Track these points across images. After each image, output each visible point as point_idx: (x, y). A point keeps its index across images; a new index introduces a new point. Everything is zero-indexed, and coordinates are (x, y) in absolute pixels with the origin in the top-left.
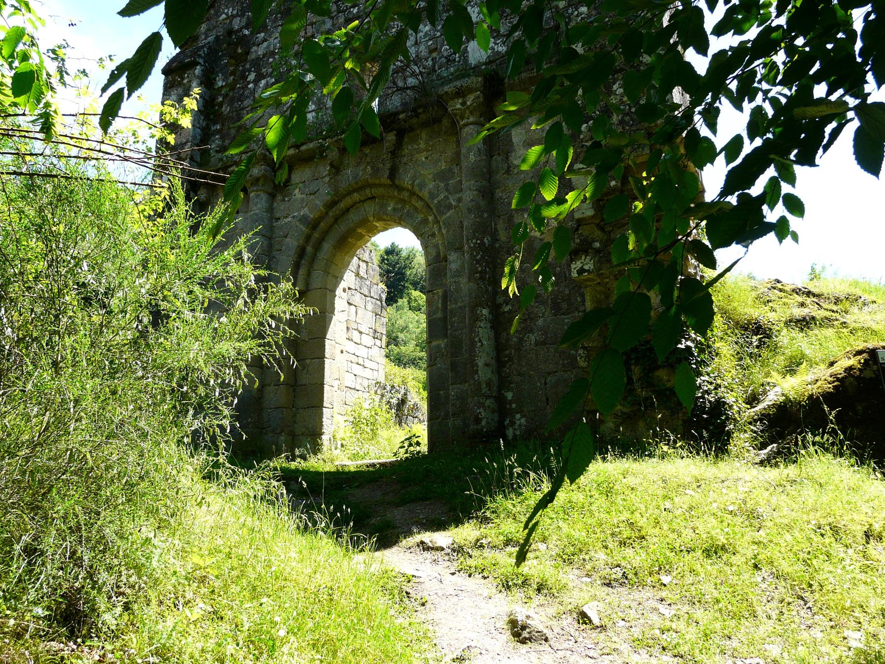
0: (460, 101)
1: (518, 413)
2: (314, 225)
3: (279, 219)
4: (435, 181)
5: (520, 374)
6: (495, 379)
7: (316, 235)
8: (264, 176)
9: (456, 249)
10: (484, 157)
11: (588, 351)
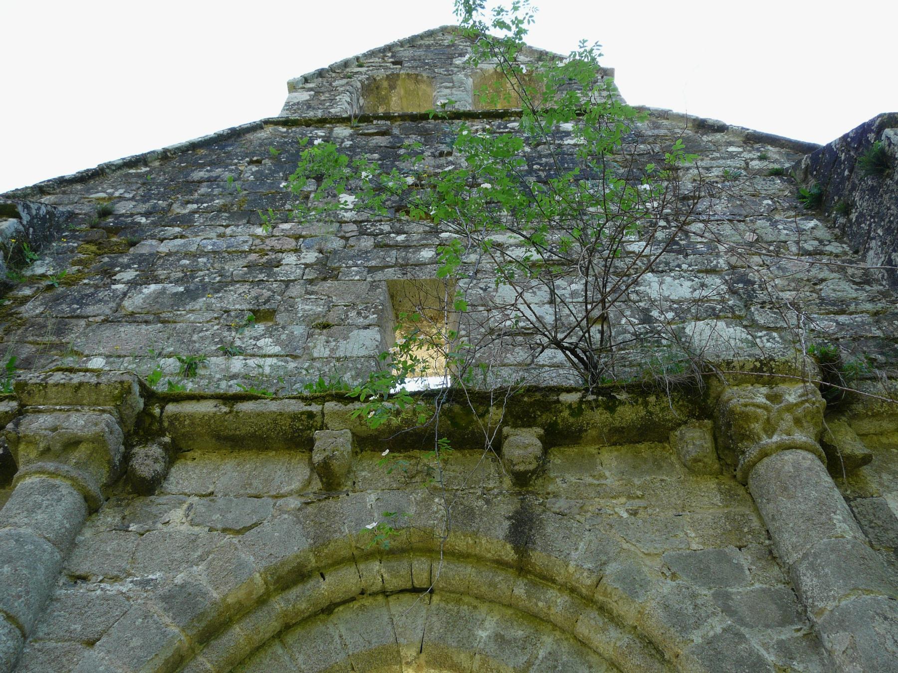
3: (84, 579)
4: (674, 576)
8: (98, 440)
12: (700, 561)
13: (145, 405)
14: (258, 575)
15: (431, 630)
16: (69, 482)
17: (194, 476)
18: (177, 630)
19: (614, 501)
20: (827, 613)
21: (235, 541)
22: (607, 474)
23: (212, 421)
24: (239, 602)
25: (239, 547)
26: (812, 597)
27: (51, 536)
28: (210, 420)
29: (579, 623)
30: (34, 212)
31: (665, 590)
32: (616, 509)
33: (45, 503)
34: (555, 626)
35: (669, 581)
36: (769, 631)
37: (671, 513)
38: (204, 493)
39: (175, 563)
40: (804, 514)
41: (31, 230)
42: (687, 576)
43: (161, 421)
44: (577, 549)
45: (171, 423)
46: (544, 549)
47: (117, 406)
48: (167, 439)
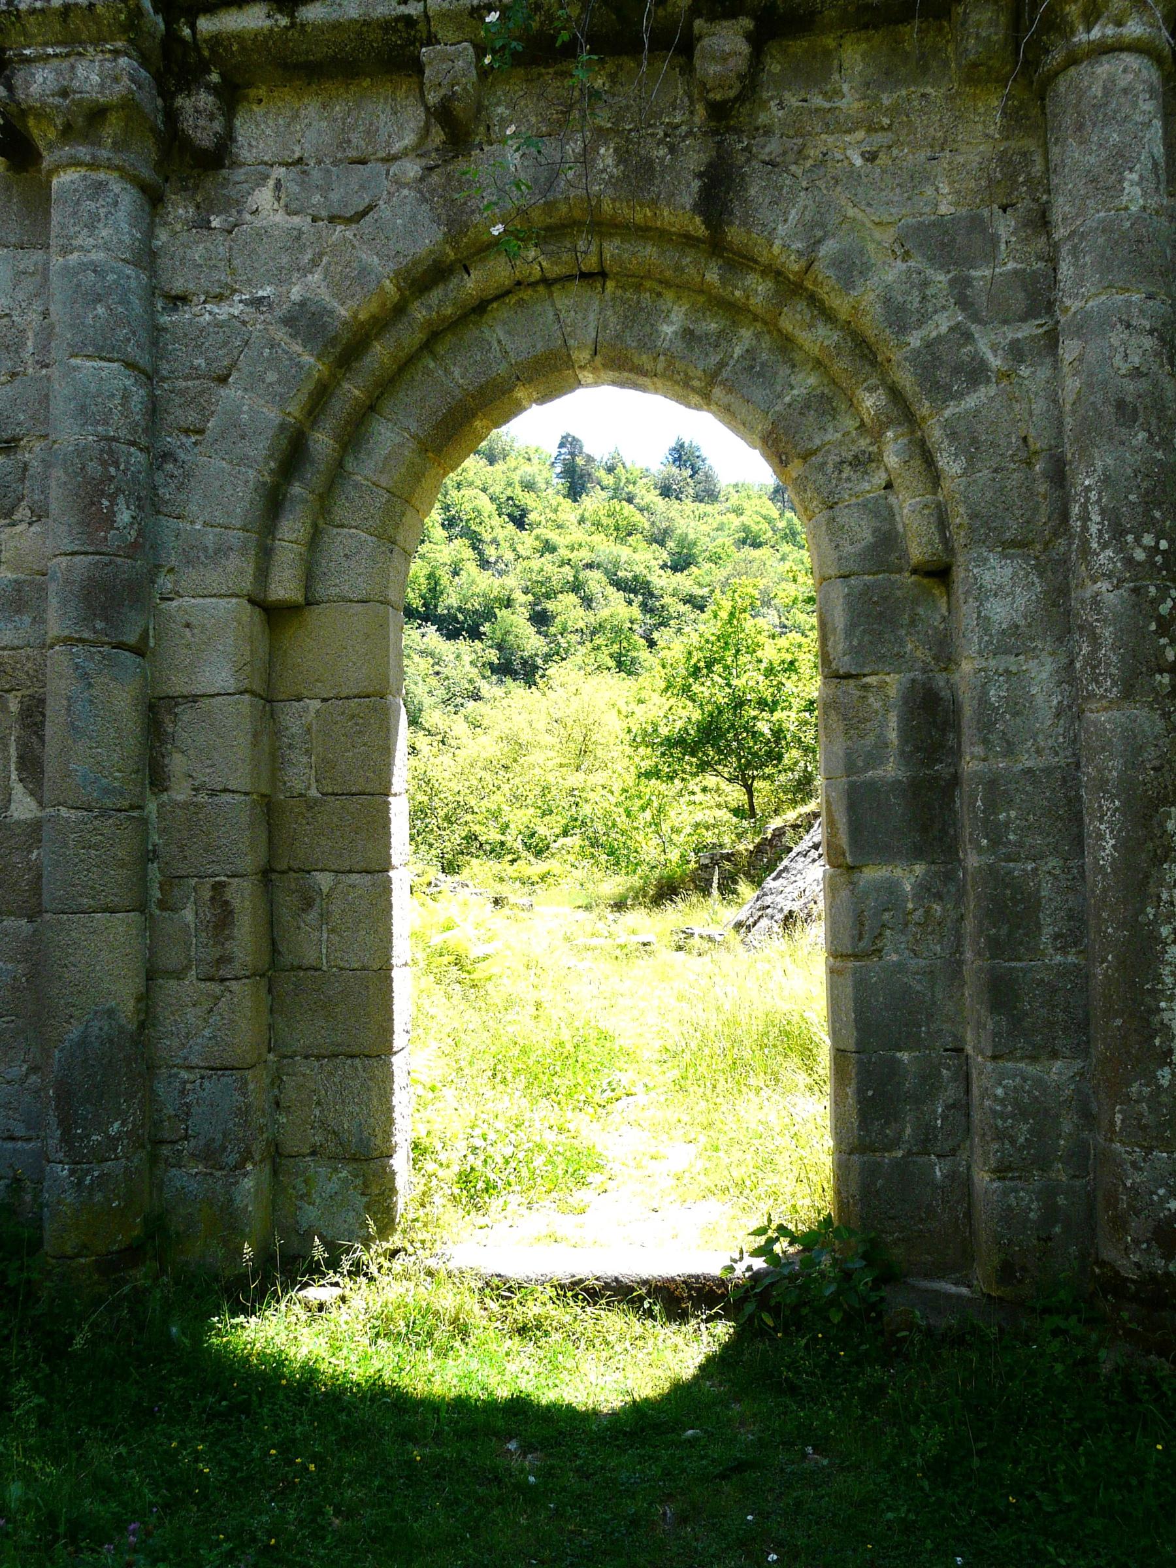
4: (907, 256)
7: (353, 390)
8: (128, 105)
9: (1006, 545)
12: (946, 233)
13: (168, 23)
14: (388, 282)
15: (605, 327)
16: (116, 174)
17: (269, 131)
18: (312, 360)
19: (847, 138)
20: (1070, 314)
21: (349, 235)
22: (845, 87)
23: (271, 42)
24: (373, 317)
25: (356, 243)
26: (1063, 291)
27: (127, 256)
28: (267, 42)
29: (783, 317)
31: (890, 278)
32: (849, 152)
33: (102, 211)
34: (756, 318)
35: (899, 262)
36: (1005, 328)
37: (922, 156)
38: (290, 161)
39: (284, 272)
40: (1089, 171)
42: (924, 255)
43: (197, 49)
44: (786, 221)
45: (212, 50)
46: (744, 223)
47: (130, 41)
48: (215, 77)
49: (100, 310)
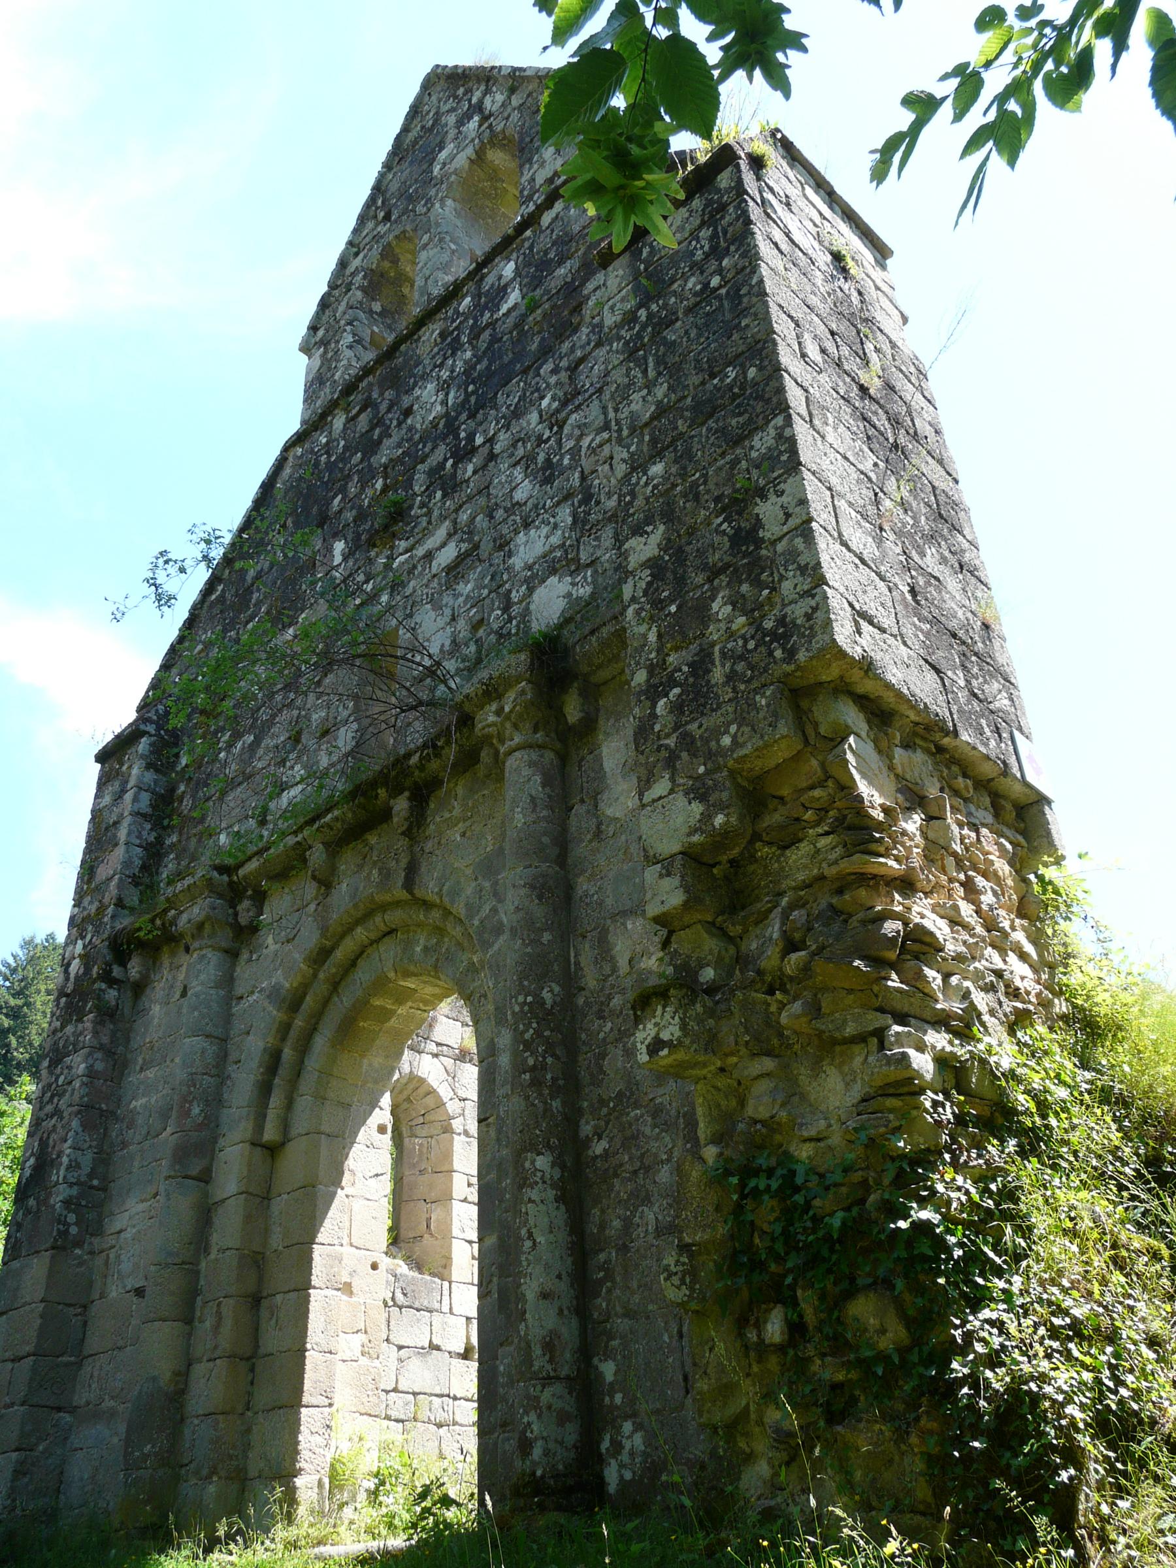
0: (494, 707)
1: (626, 1417)
2: (294, 1004)
3: (242, 998)
5: (629, 1314)
6: (569, 1331)
7: (299, 1023)
10: (545, 813)
11: (691, 1256)
24: (300, 984)
30: (155, 718)
41: (162, 732)
48: (250, 892)
49: (196, 1013)
